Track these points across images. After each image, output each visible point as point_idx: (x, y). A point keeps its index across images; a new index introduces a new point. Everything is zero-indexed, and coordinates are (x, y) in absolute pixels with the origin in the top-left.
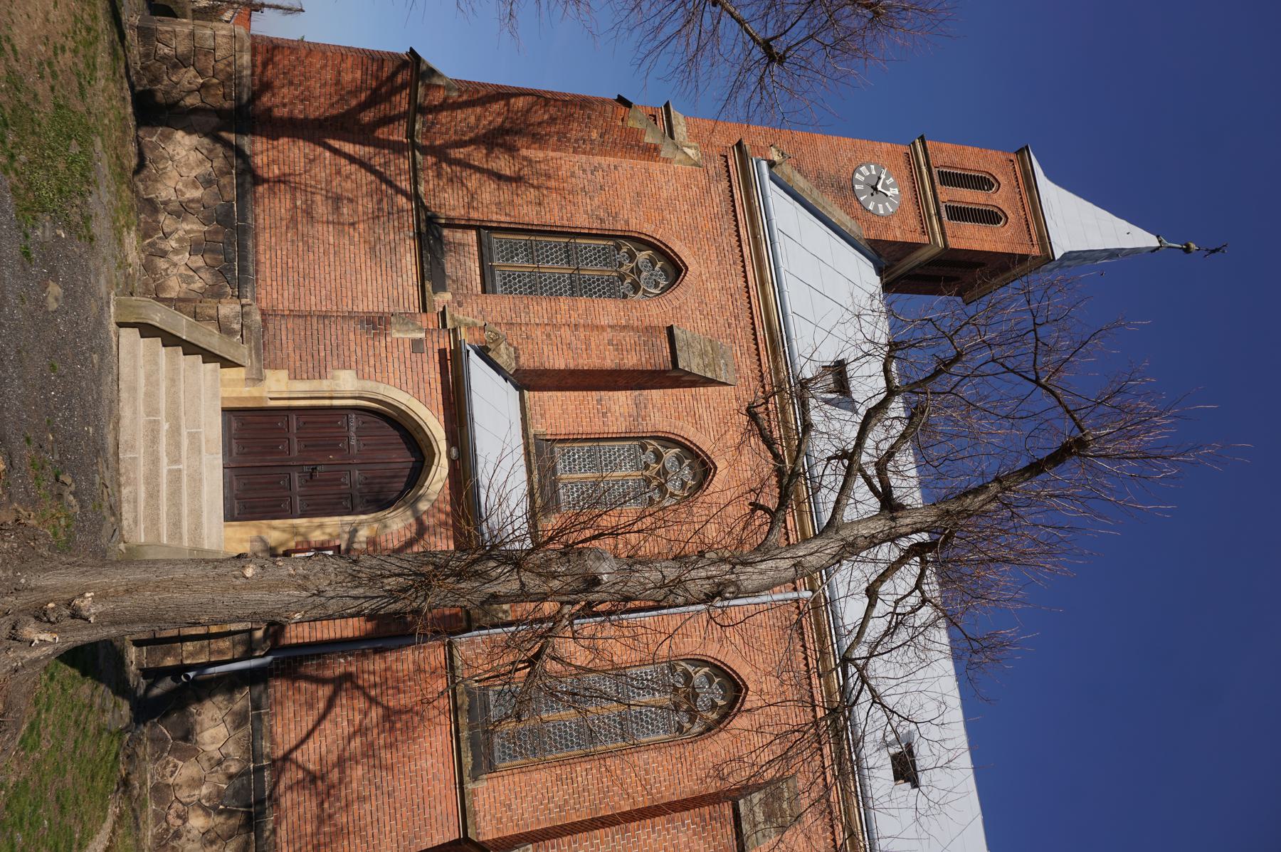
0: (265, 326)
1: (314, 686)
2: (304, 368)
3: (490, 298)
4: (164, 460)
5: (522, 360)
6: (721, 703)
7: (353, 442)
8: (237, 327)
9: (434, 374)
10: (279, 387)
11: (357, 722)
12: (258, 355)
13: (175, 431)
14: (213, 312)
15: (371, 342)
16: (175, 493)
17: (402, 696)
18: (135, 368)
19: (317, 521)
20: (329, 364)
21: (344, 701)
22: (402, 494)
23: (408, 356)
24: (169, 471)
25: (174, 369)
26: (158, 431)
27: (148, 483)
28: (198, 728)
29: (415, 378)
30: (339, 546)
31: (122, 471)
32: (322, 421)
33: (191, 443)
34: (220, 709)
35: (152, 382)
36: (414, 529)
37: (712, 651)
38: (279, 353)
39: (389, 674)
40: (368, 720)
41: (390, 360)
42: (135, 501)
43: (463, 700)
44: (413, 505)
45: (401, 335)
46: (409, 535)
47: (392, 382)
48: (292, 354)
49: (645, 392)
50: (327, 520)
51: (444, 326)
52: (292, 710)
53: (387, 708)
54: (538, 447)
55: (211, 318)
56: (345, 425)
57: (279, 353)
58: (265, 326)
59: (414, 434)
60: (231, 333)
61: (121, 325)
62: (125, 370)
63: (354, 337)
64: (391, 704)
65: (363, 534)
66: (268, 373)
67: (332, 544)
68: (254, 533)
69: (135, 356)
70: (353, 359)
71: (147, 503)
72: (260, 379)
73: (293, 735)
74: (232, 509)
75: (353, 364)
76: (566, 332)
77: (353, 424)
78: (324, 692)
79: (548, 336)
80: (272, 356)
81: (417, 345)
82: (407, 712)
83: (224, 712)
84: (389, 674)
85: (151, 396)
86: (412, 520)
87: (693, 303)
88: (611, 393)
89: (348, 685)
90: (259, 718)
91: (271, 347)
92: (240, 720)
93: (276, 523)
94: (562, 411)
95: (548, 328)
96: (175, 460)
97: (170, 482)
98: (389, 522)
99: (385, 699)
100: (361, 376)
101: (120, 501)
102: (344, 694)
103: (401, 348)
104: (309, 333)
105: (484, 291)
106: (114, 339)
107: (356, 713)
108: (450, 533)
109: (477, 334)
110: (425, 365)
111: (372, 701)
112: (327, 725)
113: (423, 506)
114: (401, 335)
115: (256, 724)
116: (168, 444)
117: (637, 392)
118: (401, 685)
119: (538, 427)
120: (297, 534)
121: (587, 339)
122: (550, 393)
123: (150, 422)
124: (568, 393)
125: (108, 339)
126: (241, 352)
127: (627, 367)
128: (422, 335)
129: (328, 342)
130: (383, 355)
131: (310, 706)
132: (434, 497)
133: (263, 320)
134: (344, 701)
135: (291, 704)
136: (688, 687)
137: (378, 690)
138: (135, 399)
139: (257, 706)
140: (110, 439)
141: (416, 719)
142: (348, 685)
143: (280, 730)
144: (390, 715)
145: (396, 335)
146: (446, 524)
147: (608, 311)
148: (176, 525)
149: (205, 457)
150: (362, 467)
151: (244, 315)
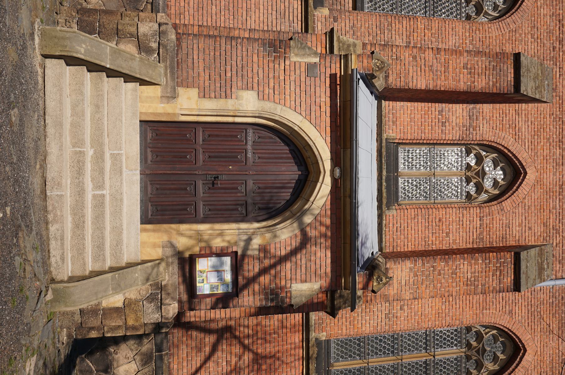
0: (179, 45)
1: (202, 335)
2: (212, 87)
3: (360, 15)
4: (89, 185)
5: (391, 79)
6: (502, 357)
7: (250, 155)
8: (154, 45)
9: (324, 98)
10: (190, 105)
11: (233, 363)
12: (172, 73)
13: (99, 157)
14: (133, 29)
15: (271, 65)
16: (99, 218)
17: (268, 345)
18: (61, 102)
19: (218, 226)
20: (234, 84)
21: (224, 347)
22: (290, 204)
23: (303, 79)
24: (94, 196)
25: (98, 95)
26: (84, 163)
27: (74, 214)
28: (115, 364)
29: (308, 101)
30: (236, 253)
31: (50, 208)
32: (224, 135)
33: (113, 164)
34: (132, 350)
35: (78, 114)
36: (299, 239)
37: (504, 322)
38: (191, 71)
39: (259, 328)
40: (241, 362)
41: (287, 83)
42: (62, 239)
43: (314, 351)
44: (299, 216)
45: (298, 59)
46: (294, 244)
47: (288, 104)
48: (202, 74)
49: (478, 106)
50: (225, 226)
51: (332, 51)
52: (185, 352)
53: (256, 354)
54: (388, 148)
55: (132, 36)
56: (244, 139)
57: (191, 71)
58: (179, 45)
59: (303, 151)
60: (149, 51)
61: (46, 56)
62: (51, 104)
63: (257, 58)
64: (260, 351)
65: (257, 242)
66: (181, 91)
67: (230, 250)
68: (165, 238)
69: (61, 90)
70: (256, 80)
71: (74, 233)
72: (172, 96)
73: (185, 371)
74: (146, 216)
75: (255, 85)
76: (429, 55)
77: (250, 138)
78: (210, 339)
79: (415, 58)
80: (185, 74)
81: (310, 67)
82: (271, 357)
83: (135, 353)
84: (259, 328)
85: (77, 126)
86: (297, 232)
87: (526, 28)
88: (451, 105)
89: (229, 335)
90: (161, 358)
91: (184, 66)
92: (146, 359)
93: (184, 227)
94: (407, 117)
95: (415, 50)
96: (99, 185)
97: (95, 207)
98: (278, 233)
99: (255, 347)
100: (262, 97)
101: (48, 238)
102: (224, 341)
103: (298, 72)
104: (218, 54)
105: (355, 8)
106: (40, 71)
107: (233, 357)
108: (329, 243)
109: (365, 61)
110: (318, 89)
111: (246, 348)
112: (211, 364)
113: (308, 219)
114: (298, 59)
115: (158, 363)
116: (93, 170)
117: (472, 106)
118: (268, 337)
119: (390, 133)
120: (200, 241)
121: (447, 62)
122: (402, 103)
123: (76, 153)
124: (416, 104)
125: (33, 73)
126: (159, 72)
127: (476, 89)
128: (317, 60)
129: (234, 63)
130: (282, 78)
131: (199, 350)
132: (317, 212)
133: (178, 39)
134: (224, 347)
135: (185, 347)
136: (479, 343)
137: (251, 340)
138: (61, 135)
139: (159, 349)
140: (36, 181)
141: (277, 363)
142: (229, 335)
143: (176, 366)
144: (258, 359)
145: (294, 59)
146: (325, 236)
147: (455, 32)
148: (100, 247)
149: (125, 172)
150: (256, 177)
151: (161, 34)
